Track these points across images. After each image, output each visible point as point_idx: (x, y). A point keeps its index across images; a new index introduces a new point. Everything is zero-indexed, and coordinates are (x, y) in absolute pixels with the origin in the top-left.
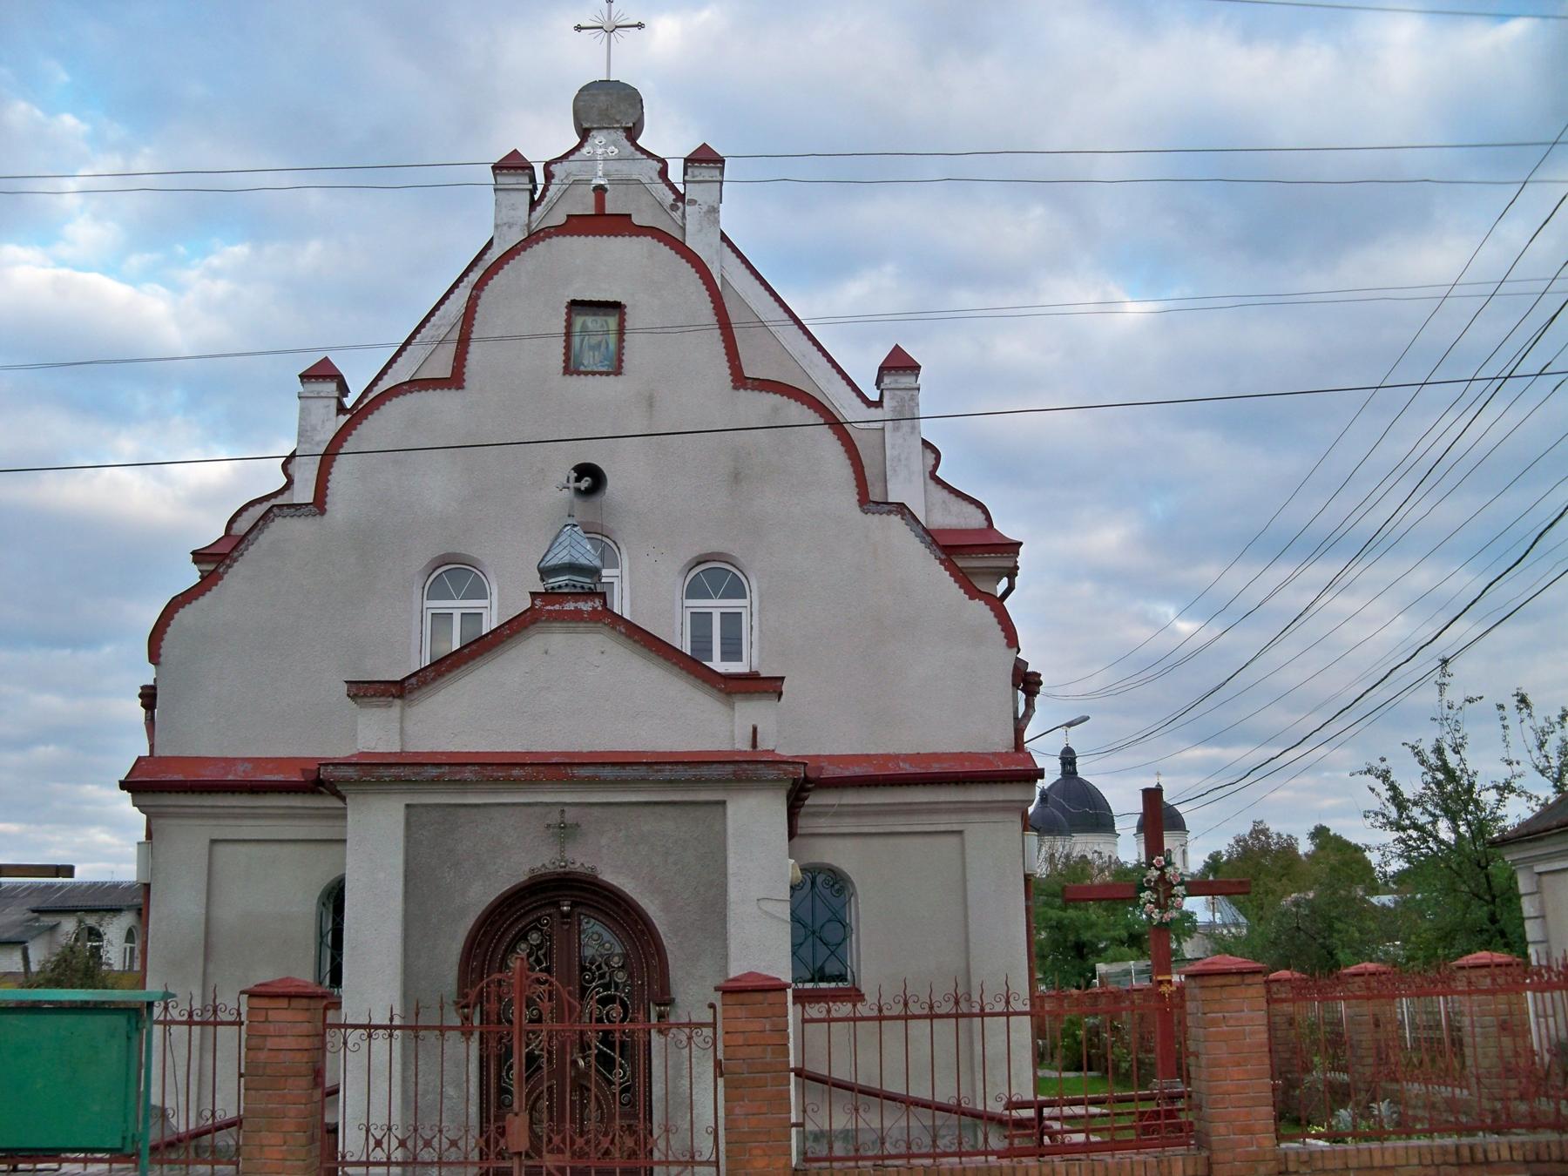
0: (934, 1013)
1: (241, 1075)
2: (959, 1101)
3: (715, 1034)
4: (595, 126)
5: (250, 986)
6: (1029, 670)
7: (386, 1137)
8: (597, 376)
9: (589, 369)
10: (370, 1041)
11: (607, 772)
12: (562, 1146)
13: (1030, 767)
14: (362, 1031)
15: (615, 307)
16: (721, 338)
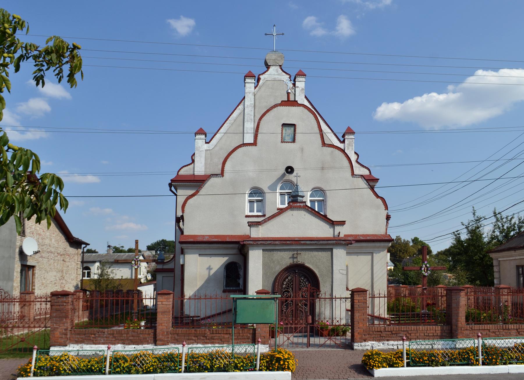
2: (379, 315)
9: (287, 141)
11: (308, 242)
13: (390, 238)
15: (294, 125)
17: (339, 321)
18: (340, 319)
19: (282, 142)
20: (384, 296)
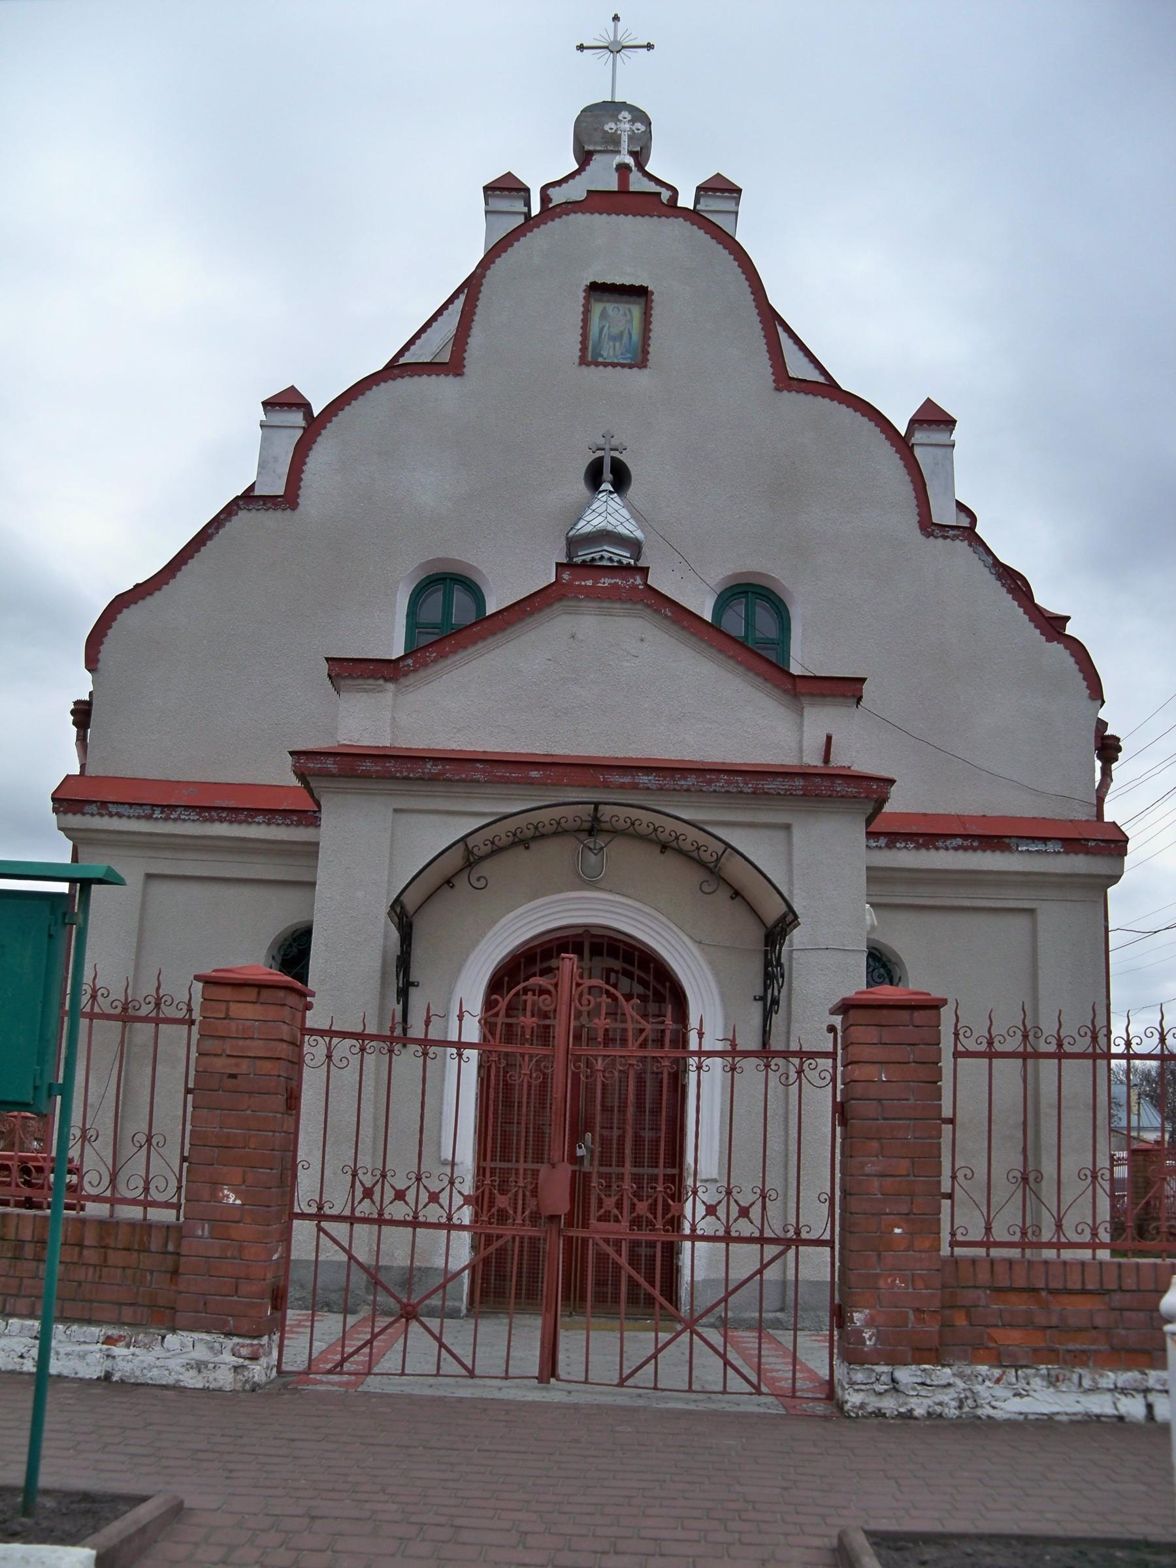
0: (1131, 1052)
1: (188, 1091)
3: (835, 1067)
4: (599, 148)
5: (207, 970)
6: (1107, 733)
7: (379, 1185)
8: (619, 368)
10: (363, 1054)
12: (635, 1201)
14: (354, 1042)
15: (640, 293)
16: (763, 333)
17: (755, 1213)
18: (764, 1197)
19: (583, 361)
20: (983, 1047)
